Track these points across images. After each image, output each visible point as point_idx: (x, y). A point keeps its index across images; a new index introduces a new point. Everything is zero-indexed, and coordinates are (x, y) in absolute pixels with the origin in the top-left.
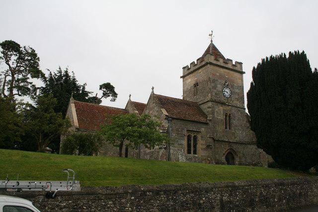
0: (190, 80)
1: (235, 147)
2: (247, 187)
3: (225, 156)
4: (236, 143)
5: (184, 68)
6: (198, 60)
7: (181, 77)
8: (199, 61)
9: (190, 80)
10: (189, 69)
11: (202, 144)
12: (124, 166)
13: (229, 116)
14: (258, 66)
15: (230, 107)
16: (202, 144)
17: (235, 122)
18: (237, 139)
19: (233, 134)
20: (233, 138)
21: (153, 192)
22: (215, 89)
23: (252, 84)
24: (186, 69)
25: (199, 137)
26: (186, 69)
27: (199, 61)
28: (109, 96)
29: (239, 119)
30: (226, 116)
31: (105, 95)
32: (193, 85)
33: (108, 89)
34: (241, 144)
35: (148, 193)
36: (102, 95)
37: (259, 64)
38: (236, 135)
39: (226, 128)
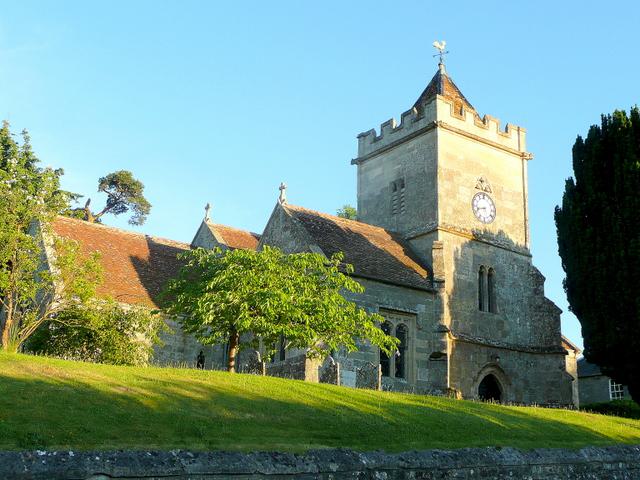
0: (378, 171)
1: (502, 361)
2: (609, 466)
3: (478, 384)
4: (508, 349)
5: (361, 136)
6: (404, 115)
7: (353, 162)
8: (407, 119)
9: (378, 171)
10: (376, 140)
11: (419, 350)
12: (141, 400)
13: (490, 275)
14: (359, 202)
15: (491, 249)
16: (419, 350)
17: (503, 292)
18: (509, 340)
19: (500, 323)
20: (500, 334)
21: (389, 472)
22: (454, 197)
23: (569, 182)
24: (369, 139)
25: (411, 327)
26: (369, 139)
27: (407, 119)
28: (124, 209)
29: (514, 285)
30: (481, 273)
31: (113, 205)
32: (387, 184)
33: (122, 189)
34: (522, 350)
35: (377, 475)
36: (105, 205)
37: (594, 130)
38: (507, 327)
39: (481, 308)
